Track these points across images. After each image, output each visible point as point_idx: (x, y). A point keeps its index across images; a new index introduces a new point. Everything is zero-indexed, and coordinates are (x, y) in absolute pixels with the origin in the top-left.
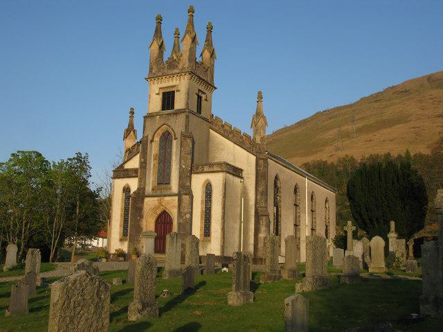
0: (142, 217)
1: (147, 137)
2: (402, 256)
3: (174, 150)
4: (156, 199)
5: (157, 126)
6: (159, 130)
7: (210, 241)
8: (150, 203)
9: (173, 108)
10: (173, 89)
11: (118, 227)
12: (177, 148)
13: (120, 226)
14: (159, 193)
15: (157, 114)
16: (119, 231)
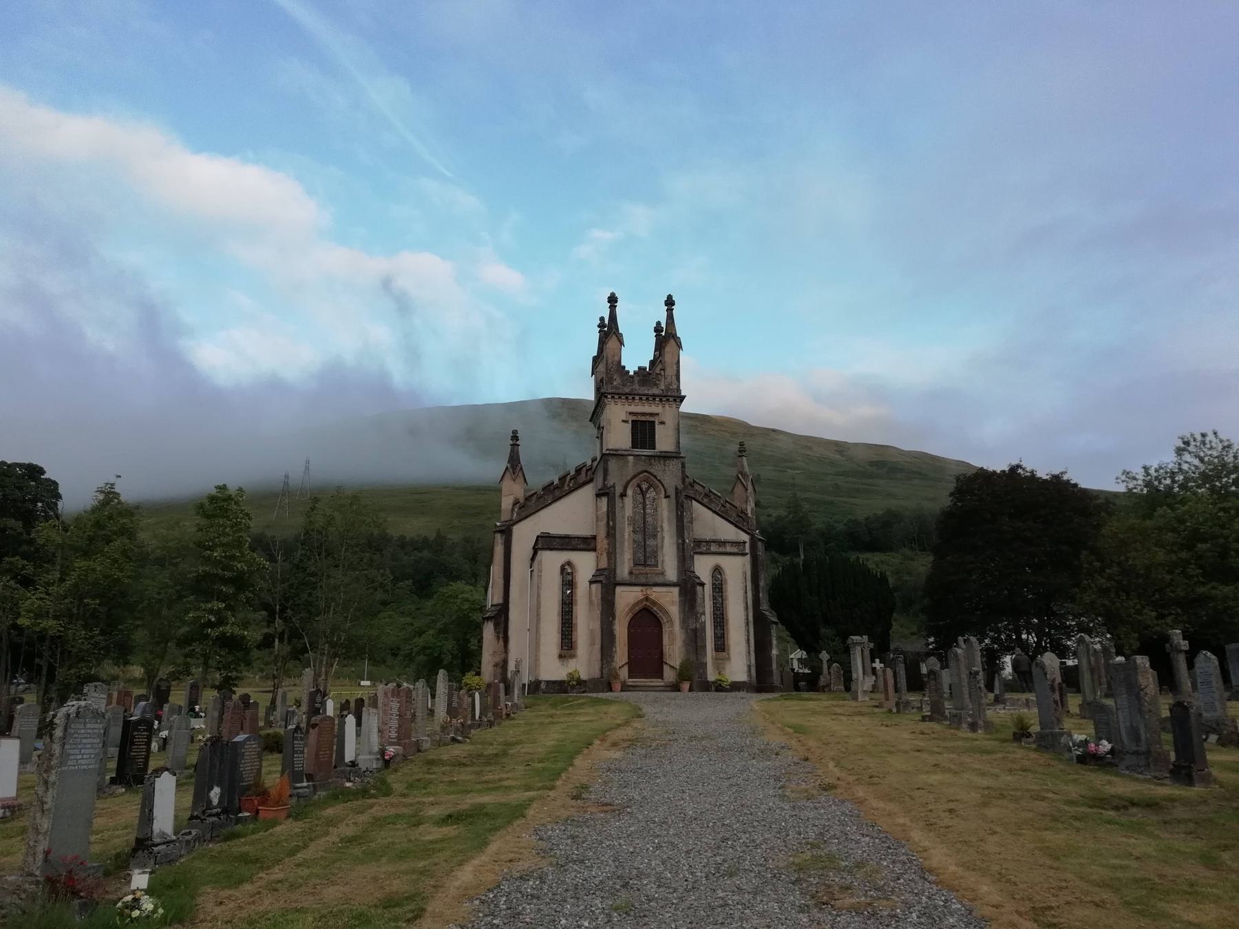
0: (614, 618)
1: (614, 486)
4: (638, 589)
6: (634, 480)
9: (654, 448)
10: (652, 419)
14: (643, 580)
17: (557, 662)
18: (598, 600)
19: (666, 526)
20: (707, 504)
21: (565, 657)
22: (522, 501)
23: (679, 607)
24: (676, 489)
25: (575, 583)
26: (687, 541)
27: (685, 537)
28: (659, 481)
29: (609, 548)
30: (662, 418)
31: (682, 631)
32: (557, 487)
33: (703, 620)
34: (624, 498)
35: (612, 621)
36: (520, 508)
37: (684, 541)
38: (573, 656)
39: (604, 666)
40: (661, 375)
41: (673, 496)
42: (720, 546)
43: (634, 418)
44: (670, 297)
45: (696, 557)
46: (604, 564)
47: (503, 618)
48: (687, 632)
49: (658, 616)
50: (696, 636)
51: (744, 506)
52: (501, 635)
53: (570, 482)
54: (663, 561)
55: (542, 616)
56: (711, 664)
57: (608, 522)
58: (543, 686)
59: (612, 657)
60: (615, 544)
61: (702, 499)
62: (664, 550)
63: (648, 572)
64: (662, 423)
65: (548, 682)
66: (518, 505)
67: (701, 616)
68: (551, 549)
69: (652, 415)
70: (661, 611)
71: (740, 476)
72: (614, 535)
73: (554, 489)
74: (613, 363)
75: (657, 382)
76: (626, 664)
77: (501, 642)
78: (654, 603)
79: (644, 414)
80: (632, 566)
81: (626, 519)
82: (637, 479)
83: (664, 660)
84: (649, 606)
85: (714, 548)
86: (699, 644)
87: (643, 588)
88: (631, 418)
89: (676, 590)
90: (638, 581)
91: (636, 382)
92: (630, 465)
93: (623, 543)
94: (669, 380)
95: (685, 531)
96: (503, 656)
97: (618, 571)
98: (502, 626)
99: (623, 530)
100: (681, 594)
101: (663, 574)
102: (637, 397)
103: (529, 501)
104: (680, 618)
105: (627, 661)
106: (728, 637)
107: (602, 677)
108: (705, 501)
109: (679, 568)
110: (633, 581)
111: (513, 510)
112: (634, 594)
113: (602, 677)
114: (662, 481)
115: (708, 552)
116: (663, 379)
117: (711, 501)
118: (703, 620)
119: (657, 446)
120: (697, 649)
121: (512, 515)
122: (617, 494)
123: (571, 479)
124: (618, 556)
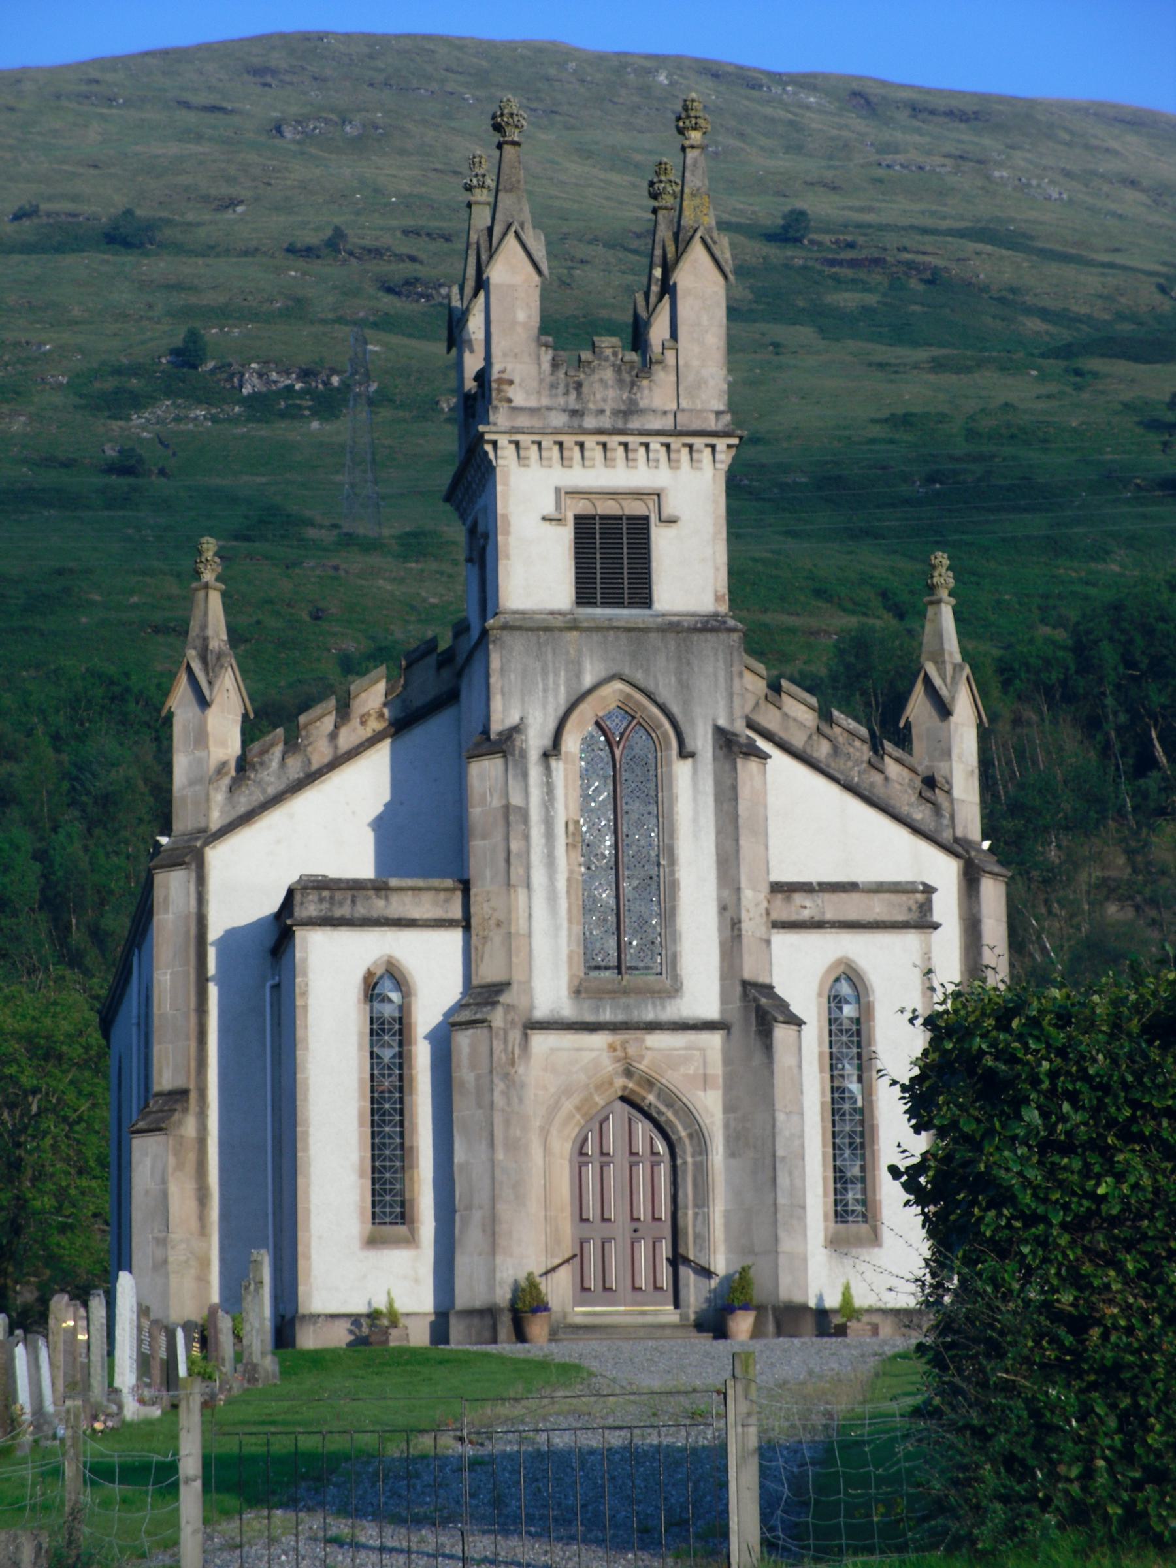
4: (600, 1040)
10: (635, 508)
28: (663, 709)
49: (662, 1119)
84: (632, 1091)
110: (589, 1017)
112: (588, 1056)
122: (534, 755)
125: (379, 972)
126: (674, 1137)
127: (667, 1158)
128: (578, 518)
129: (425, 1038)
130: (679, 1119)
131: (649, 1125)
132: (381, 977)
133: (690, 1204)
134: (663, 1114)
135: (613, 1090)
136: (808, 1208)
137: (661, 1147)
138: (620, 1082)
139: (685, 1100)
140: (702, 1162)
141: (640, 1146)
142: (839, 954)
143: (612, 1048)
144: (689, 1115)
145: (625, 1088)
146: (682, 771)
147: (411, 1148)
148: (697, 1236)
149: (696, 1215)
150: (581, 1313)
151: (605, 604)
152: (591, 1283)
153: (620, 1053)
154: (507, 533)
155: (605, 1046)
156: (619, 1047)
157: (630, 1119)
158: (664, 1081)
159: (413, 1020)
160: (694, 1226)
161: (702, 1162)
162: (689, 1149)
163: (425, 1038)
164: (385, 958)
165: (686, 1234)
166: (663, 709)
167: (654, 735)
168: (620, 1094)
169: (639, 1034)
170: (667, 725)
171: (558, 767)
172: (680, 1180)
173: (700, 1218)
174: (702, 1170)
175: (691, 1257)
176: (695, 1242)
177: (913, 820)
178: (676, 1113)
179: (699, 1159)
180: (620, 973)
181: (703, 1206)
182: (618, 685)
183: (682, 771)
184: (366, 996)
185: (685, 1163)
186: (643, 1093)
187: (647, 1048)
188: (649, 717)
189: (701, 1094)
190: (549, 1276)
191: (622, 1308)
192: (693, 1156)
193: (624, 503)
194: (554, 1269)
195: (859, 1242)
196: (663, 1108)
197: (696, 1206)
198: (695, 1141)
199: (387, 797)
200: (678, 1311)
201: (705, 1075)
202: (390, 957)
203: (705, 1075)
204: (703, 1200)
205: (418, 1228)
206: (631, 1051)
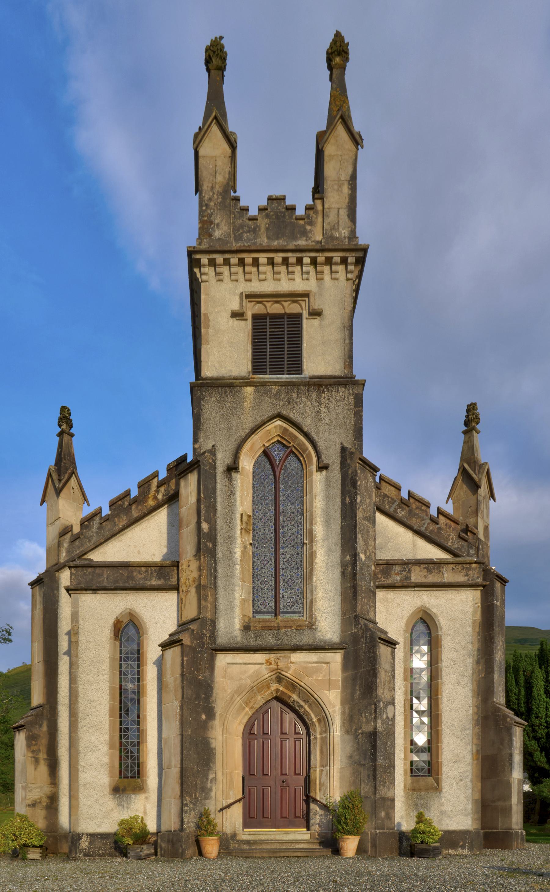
0: (211, 714)
1: (213, 452)
2: (344, 162)
3: (319, 504)
4: (260, 657)
5: (248, 422)
6: (255, 438)
7: (438, 788)
8: (235, 670)
9: (299, 370)
10: (292, 308)
11: (104, 748)
12: (328, 498)
13: (111, 747)
14: (269, 639)
15: (246, 382)
16: (106, 760)
17: (110, 802)
18: (175, 681)
19: (319, 530)
20: (404, 519)
21: (124, 790)
22: (76, 529)
23: (342, 692)
24: (343, 449)
25: (143, 652)
26: (362, 556)
27: (359, 550)
28: (307, 435)
29: (200, 576)
30: (316, 305)
31: (347, 737)
32: (135, 501)
33: (390, 716)
34: (234, 475)
35: (206, 722)
36: (72, 541)
37: (355, 556)
38: (140, 788)
39: (185, 808)
40: (316, 212)
41: (335, 468)
42: (430, 571)
43: (258, 309)
44: (338, 39)
45: (380, 594)
46: (191, 612)
47: (45, 728)
48: (356, 737)
49: (302, 711)
50: (374, 747)
51: (471, 521)
52: (42, 756)
53: (157, 491)
54: (312, 602)
55: (81, 716)
56: (403, 799)
57: (199, 524)
58: (84, 843)
59: (206, 792)
60: (216, 571)
61: (395, 511)
62: (315, 578)
63: (281, 624)
64: (316, 314)
65: (92, 836)
66: (68, 536)
67: (386, 706)
68: (95, 590)
69: (294, 296)
70: (306, 701)
71: (466, 465)
72: (213, 553)
73: (130, 505)
74: (212, 188)
75: (308, 228)
76: (239, 801)
77: (43, 768)
78: (293, 686)
79: (277, 297)
80: (251, 615)
81: (238, 516)
82: (261, 433)
83: (312, 794)
84: (283, 692)
85: (417, 575)
86: (380, 761)
87: (272, 656)
88: (252, 309)
89: (337, 657)
90: (260, 643)
91: (263, 229)
92: (248, 404)
93: (231, 567)
94: (332, 218)
95: (359, 536)
96: (47, 790)
97: (221, 625)
98: (44, 741)
99: (230, 540)
100: (345, 666)
101: (311, 626)
102: (263, 258)
103: (87, 527)
104: (343, 713)
105: (240, 796)
106: (438, 747)
107: (182, 829)
108: (401, 514)
109: (344, 613)
110: (252, 643)
111: (59, 545)
112: (252, 669)
113: (182, 829)
114: (313, 434)
115: (405, 583)
116: (320, 219)
117: (411, 513)
118: (390, 716)
119: (305, 365)
120: (375, 771)
121: (59, 555)
122: (220, 469)
123: (159, 486)
124: (221, 592)
125: (125, 621)
126: (309, 722)
127: (305, 735)
128: (256, 318)
129: (154, 663)
130: (312, 710)
131: (293, 715)
132: (127, 625)
133: (318, 765)
134: (302, 707)
135: (269, 692)
136: (396, 768)
137: (301, 728)
138: (274, 686)
139: (316, 696)
140: (326, 737)
141: (287, 728)
142: (419, 604)
143: (268, 662)
144: (317, 705)
145: (277, 690)
146: (318, 478)
147: (143, 730)
148: (322, 785)
149: (322, 771)
150: (246, 834)
151: (271, 373)
152: (254, 813)
153: (273, 666)
154: (208, 327)
155: (264, 662)
156: (273, 662)
157: (282, 712)
158: (302, 684)
159: (145, 650)
160: (320, 778)
161: (326, 737)
162: (318, 729)
163: (154, 663)
164: (128, 611)
165: (315, 783)
166: (307, 435)
167: (301, 459)
168: (275, 695)
169: (286, 654)
170: (310, 448)
171: (237, 478)
172: (312, 749)
173: (324, 773)
174: (326, 742)
175: (318, 799)
176: (320, 789)
177: (428, 679)
178: (310, 706)
179: (324, 735)
180: (276, 615)
181: (326, 766)
182: (278, 423)
183: (318, 478)
184: (115, 635)
185: (316, 738)
186: (290, 693)
187: (292, 663)
188: (298, 445)
189: (326, 692)
190: (224, 811)
191: (275, 830)
192: (321, 734)
193: (286, 304)
194: (228, 806)
195: (428, 789)
196: (302, 703)
197: (322, 766)
198: (323, 723)
199: (165, 550)
200: (309, 832)
201: (330, 679)
202: (130, 609)
203: (330, 679)
204: (326, 762)
205: (146, 780)
206: (281, 665)
